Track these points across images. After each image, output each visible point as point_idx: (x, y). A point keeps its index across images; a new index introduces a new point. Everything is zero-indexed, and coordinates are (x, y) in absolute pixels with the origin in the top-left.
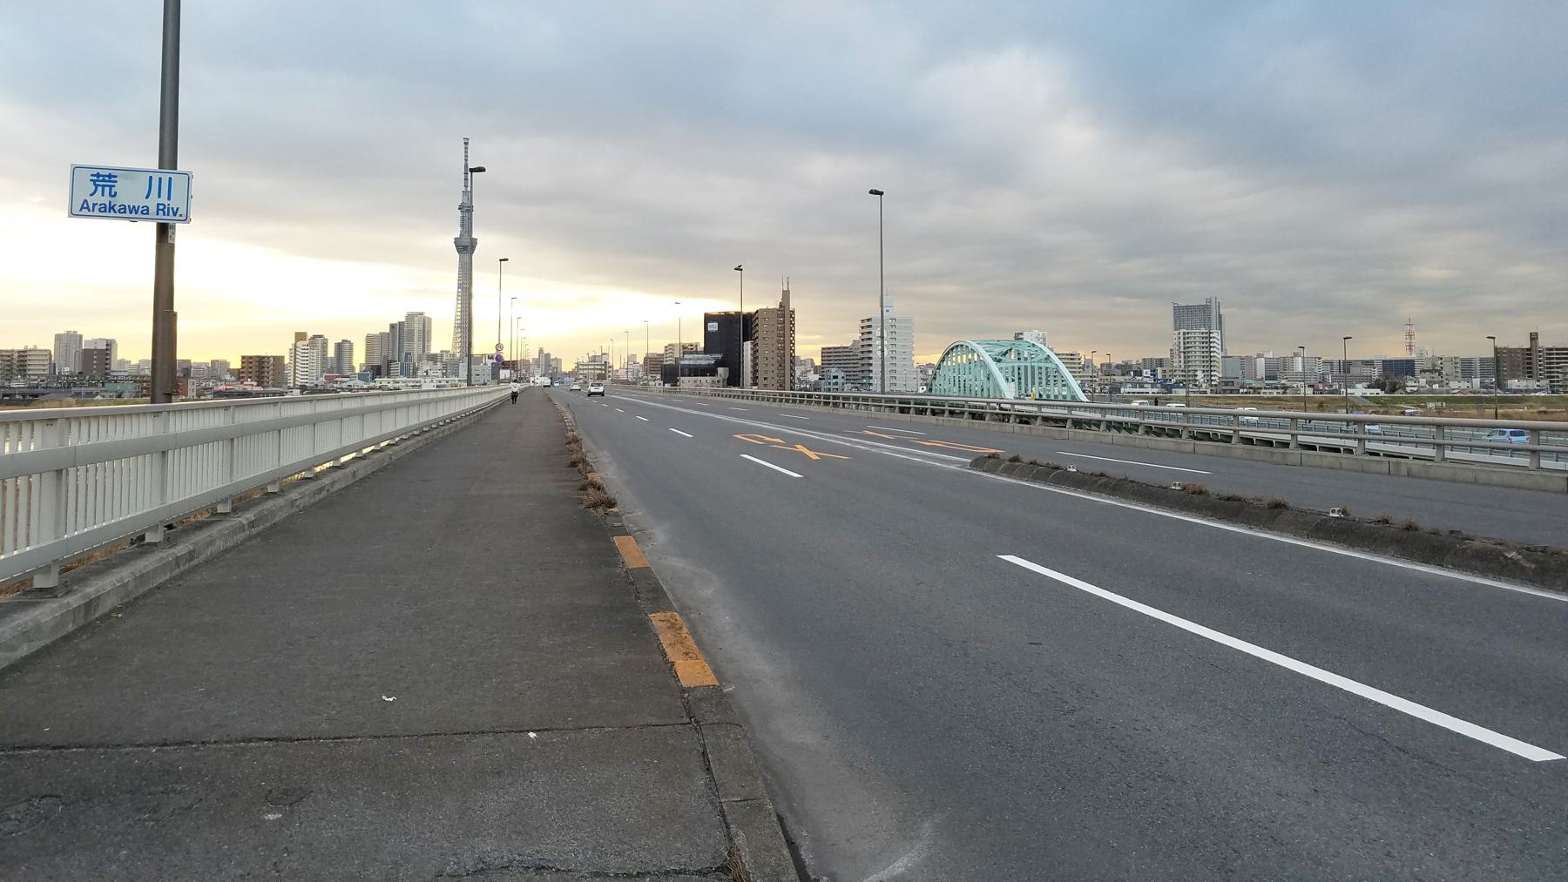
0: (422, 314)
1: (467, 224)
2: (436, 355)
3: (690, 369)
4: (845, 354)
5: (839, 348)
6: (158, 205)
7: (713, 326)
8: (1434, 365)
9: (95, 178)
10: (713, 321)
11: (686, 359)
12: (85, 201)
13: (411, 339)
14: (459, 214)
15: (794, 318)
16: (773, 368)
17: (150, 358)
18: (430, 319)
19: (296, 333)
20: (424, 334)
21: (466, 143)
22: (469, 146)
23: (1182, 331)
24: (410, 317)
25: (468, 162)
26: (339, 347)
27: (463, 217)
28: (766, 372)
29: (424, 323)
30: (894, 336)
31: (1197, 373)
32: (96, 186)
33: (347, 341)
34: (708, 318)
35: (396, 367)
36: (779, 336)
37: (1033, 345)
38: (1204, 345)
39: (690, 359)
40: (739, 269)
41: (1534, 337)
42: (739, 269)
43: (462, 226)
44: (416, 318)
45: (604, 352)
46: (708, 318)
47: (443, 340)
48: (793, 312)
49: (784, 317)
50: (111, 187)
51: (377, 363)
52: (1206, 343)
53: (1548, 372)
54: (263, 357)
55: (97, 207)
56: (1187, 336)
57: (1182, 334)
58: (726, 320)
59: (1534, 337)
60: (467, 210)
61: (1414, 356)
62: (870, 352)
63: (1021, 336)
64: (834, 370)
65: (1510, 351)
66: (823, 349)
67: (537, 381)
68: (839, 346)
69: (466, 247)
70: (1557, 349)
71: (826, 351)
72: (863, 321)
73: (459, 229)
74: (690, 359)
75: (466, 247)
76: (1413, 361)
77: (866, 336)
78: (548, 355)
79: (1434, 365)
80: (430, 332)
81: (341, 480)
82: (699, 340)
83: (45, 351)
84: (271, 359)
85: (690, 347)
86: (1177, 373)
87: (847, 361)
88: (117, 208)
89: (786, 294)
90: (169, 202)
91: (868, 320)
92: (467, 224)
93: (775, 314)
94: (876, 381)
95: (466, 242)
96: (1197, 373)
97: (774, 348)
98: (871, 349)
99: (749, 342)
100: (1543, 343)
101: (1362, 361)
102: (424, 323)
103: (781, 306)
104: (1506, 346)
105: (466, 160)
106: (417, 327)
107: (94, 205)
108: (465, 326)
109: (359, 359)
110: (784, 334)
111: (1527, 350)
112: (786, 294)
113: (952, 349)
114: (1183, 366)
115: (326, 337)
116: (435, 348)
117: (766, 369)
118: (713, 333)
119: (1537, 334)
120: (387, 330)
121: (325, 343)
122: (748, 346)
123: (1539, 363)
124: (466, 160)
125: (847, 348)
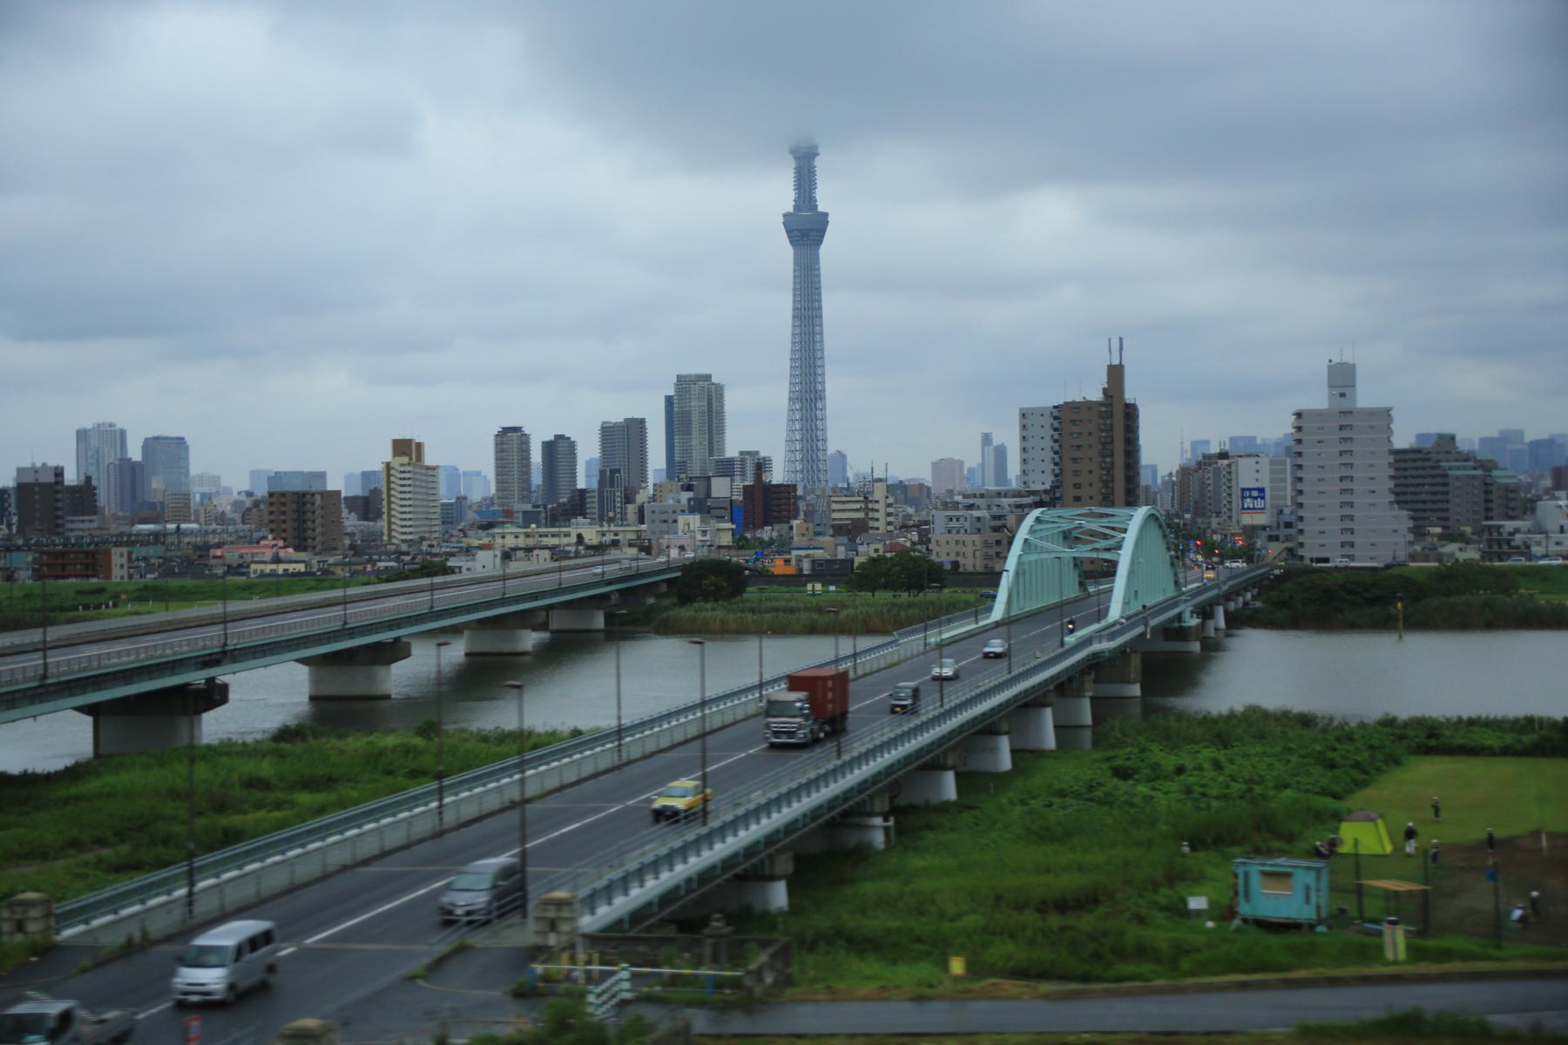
0: (708, 377)
2: (731, 461)
17: (665, 467)
19: (642, 421)
20: (710, 419)
28: (1078, 486)
29: (709, 396)
54: (304, 495)
84: (318, 498)
94: (930, 622)
102: (709, 396)
106: (696, 405)
115: (526, 430)
117: (1077, 480)
121: (524, 441)
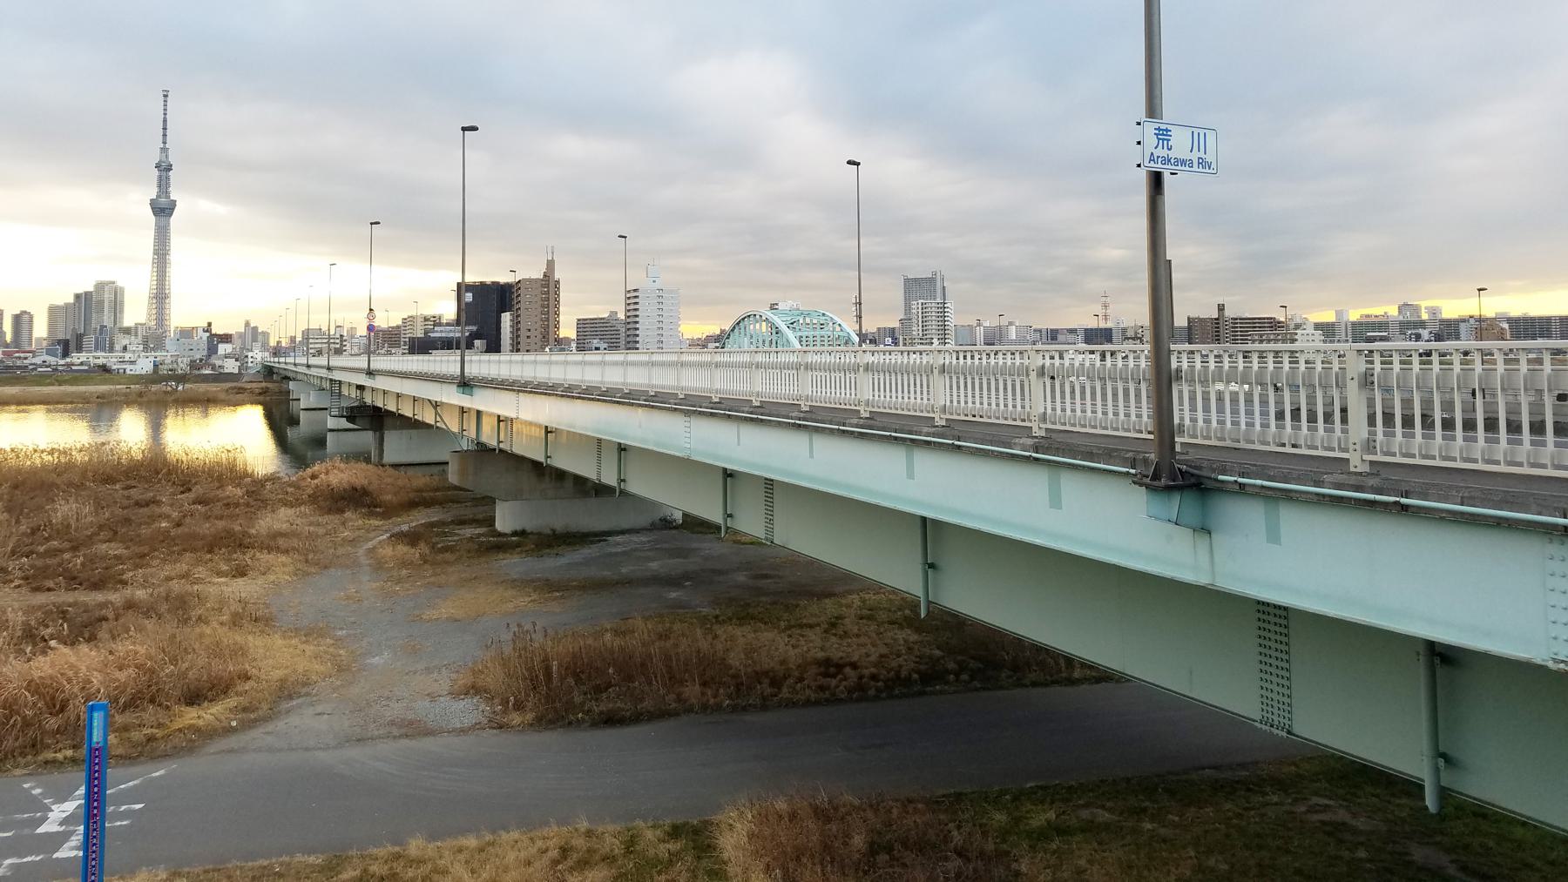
0: (114, 283)
1: (163, 184)
3: (443, 342)
4: (601, 325)
5: (596, 319)
6: (1199, 158)
7: (469, 297)
8: (1136, 333)
9: (1157, 132)
11: (437, 332)
12: (1152, 154)
15: (559, 289)
16: (537, 340)
18: (122, 290)
21: (166, 96)
22: (169, 99)
23: (920, 301)
24: (100, 286)
25: (167, 116)
26: (17, 319)
27: (160, 177)
30: (661, 306)
31: (933, 341)
32: (1159, 139)
33: (25, 312)
34: (462, 288)
35: (89, 341)
36: (543, 306)
37: (824, 314)
38: (940, 314)
39: (441, 331)
41: (1221, 308)
43: (160, 186)
47: (136, 313)
48: (558, 282)
49: (548, 287)
50: (1168, 140)
51: (61, 336)
52: (941, 308)
53: (1233, 336)
55: (1160, 160)
56: (924, 306)
57: (920, 304)
58: (481, 290)
59: (1221, 308)
60: (164, 168)
61: (1109, 325)
62: (637, 322)
63: (777, 307)
64: (595, 341)
65: (1201, 320)
66: (579, 320)
67: (255, 356)
68: (595, 317)
69: (163, 210)
70: (1240, 319)
71: (581, 322)
74: (441, 331)
75: (163, 210)
76: (1111, 329)
77: (632, 307)
78: (255, 329)
79: (1136, 333)
80: (122, 303)
82: (449, 311)
83: (1271, 318)
85: (432, 319)
86: (916, 341)
87: (605, 333)
88: (1172, 161)
89: (551, 265)
90: (1205, 156)
91: (635, 290)
92: (163, 184)
93: (539, 285)
96: (933, 341)
98: (637, 319)
99: (508, 314)
100: (1229, 313)
101: (1068, 330)
103: (545, 276)
104: (1197, 316)
105: (165, 114)
107: (1158, 157)
108: (160, 297)
109: (40, 330)
110: (548, 304)
111: (1216, 319)
112: (551, 265)
113: (743, 319)
114: (921, 335)
116: (128, 320)
119: (1223, 305)
120: (71, 300)
122: (506, 318)
123: (1225, 331)
124: (165, 114)
125: (603, 319)
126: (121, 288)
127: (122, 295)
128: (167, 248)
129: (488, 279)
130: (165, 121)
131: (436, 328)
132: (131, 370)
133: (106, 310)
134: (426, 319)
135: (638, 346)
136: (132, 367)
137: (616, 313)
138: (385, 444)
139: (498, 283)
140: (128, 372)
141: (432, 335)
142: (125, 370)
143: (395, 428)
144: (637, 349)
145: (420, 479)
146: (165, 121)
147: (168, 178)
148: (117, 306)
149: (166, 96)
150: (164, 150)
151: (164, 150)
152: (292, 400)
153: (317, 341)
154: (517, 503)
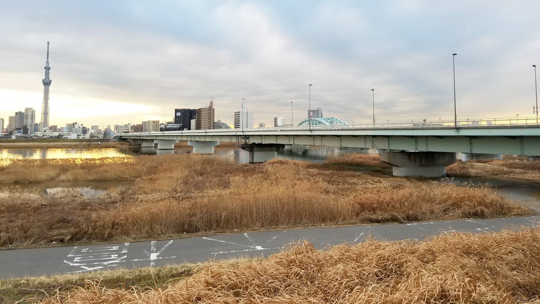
0: (32, 108)
1: (47, 74)
7: (179, 114)
10: (179, 112)
11: (169, 126)
13: (27, 118)
14: (45, 70)
18: (35, 111)
21: (48, 43)
22: (49, 44)
24: (27, 110)
25: (49, 51)
27: (46, 72)
29: (32, 112)
36: (209, 117)
39: (170, 126)
40: (373, 90)
42: (373, 90)
43: (46, 75)
44: (29, 110)
45: (129, 123)
46: (177, 111)
47: (38, 120)
48: (214, 109)
60: (47, 69)
69: (47, 83)
72: (235, 113)
73: (45, 76)
74: (170, 126)
75: (47, 83)
77: (237, 118)
80: (35, 116)
81: (497, 179)
82: (172, 119)
85: (156, 122)
89: (212, 103)
92: (47, 74)
95: (47, 81)
97: (207, 122)
99: (194, 120)
102: (32, 112)
103: (210, 107)
105: (48, 50)
106: (30, 113)
108: (46, 114)
112: (212, 103)
118: (178, 116)
124: (48, 50)
126: (34, 110)
127: (35, 113)
128: (48, 97)
129: (186, 107)
130: (48, 52)
131: (168, 125)
132: (69, 138)
133: (29, 119)
134: (154, 122)
135: (239, 126)
136: (70, 137)
137: (220, 120)
138: (254, 156)
139: (190, 109)
140: (68, 138)
141: (167, 127)
142: (67, 137)
143: (256, 151)
144: (239, 128)
145: (481, 159)
146: (48, 52)
147: (49, 72)
148: (33, 117)
149: (48, 43)
150: (48, 62)
151: (48, 62)
152: (142, 147)
153: (122, 129)
154: (404, 168)
